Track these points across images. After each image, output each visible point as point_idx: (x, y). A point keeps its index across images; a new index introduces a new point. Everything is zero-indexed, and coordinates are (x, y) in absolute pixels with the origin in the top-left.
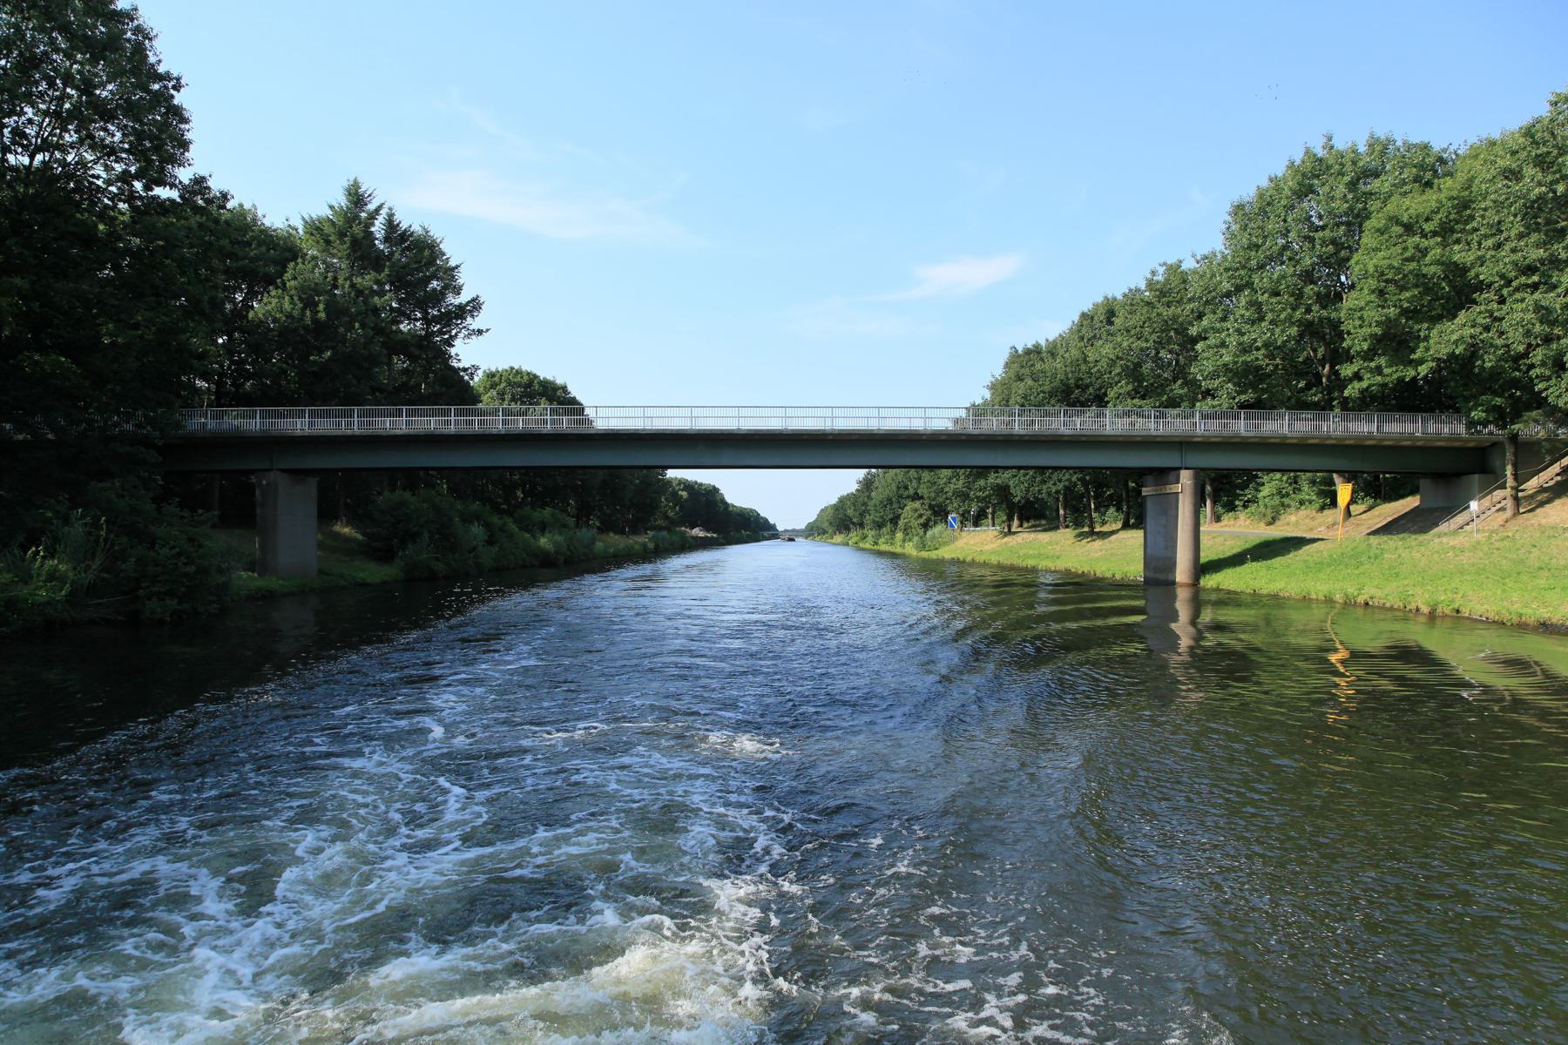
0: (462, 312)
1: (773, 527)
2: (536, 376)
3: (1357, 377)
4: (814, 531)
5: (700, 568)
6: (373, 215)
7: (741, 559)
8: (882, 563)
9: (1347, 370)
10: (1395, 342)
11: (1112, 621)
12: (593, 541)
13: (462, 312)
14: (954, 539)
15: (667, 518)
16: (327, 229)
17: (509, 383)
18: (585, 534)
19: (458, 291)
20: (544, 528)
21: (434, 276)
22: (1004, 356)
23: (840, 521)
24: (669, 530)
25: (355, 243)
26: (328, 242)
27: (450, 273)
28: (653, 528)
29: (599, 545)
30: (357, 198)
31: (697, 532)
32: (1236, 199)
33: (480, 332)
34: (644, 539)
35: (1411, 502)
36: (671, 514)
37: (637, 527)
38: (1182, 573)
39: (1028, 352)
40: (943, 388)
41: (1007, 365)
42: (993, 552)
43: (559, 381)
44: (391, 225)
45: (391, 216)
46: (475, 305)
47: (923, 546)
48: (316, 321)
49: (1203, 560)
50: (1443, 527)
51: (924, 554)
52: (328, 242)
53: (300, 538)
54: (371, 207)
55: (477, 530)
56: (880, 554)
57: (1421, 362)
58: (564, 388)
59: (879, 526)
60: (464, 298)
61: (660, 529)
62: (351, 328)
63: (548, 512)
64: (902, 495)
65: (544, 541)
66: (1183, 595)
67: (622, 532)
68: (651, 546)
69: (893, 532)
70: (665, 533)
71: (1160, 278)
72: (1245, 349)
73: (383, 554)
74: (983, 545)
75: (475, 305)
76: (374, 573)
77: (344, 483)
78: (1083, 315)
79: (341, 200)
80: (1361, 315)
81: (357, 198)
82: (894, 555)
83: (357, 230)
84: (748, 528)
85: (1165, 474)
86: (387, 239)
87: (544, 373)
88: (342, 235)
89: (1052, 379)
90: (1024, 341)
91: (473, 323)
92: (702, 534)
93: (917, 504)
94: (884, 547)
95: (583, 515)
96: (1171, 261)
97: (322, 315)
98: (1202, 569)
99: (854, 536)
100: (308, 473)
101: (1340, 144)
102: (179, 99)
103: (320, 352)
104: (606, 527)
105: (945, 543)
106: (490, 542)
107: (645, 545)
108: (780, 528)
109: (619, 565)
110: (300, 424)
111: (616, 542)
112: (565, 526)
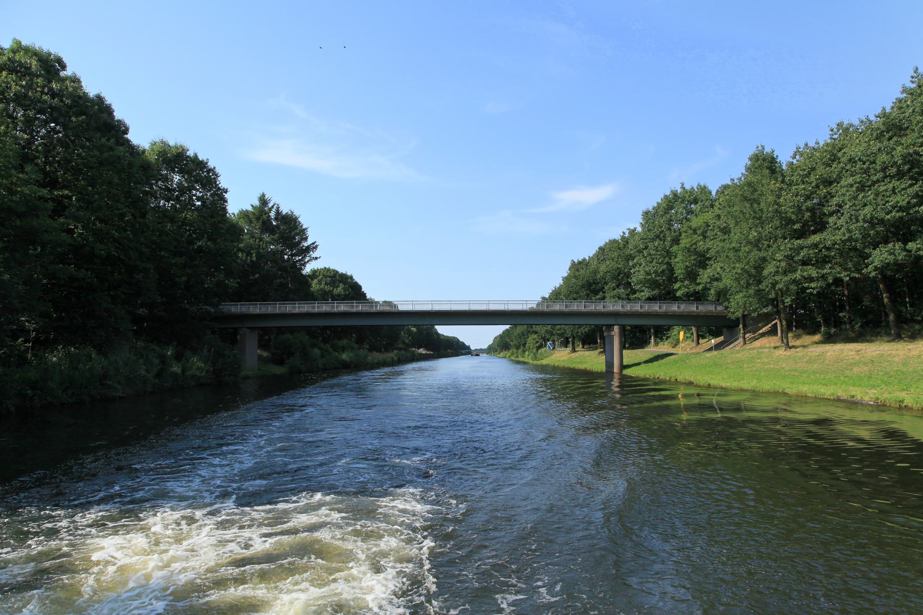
0: (308, 249)
1: (468, 348)
2: (337, 272)
3: (680, 288)
4: (491, 350)
5: (420, 369)
6: (270, 209)
7: (447, 369)
8: (519, 366)
9: (676, 286)
10: (692, 276)
11: (656, 404)
12: (366, 356)
13: (308, 249)
14: (552, 354)
15: (404, 343)
16: (251, 216)
17: (324, 276)
18: (362, 352)
19: (306, 239)
20: (343, 349)
21: (298, 234)
22: (569, 264)
23: (501, 346)
24: (405, 350)
25: (264, 223)
26: (251, 222)
27: (303, 231)
28: (396, 349)
29: (369, 358)
30: (263, 201)
31: (422, 351)
32: (645, 209)
33: (316, 258)
34: (392, 355)
35: (721, 338)
36: (407, 341)
37: (387, 348)
38: (616, 369)
39: (580, 263)
40: (532, 284)
41: (570, 269)
42: (564, 361)
43: (349, 274)
44: (278, 213)
45: (278, 208)
46: (313, 247)
47: (535, 358)
48: (252, 261)
49: (625, 363)
50: (727, 348)
51: (535, 362)
52: (251, 222)
53: (252, 355)
54: (270, 205)
55: (316, 351)
56: (518, 362)
57: (699, 284)
58: (351, 277)
59: (518, 348)
60: (309, 242)
61: (401, 349)
62: (266, 264)
63: (345, 342)
64: (524, 335)
65: (344, 356)
66: (616, 376)
67: (380, 351)
68: (396, 358)
69: (524, 351)
70: (403, 352)
71: (627, 235)
72: (648, 274)
73: (281, 363)
74: (561, 357)
75: (313, 247)
76: (278, 370)
77: (271, 334)
78: (600, 248)
79: (257, 203)
80: (680, 265)
81: (263, 201)
82: (524, 363)
83: (265, 217)
84: (456, 348)
85: (610, 327)
86: (276, 219)
87: (341, 270)
88: (258, 219)
89: (586, 281)
90: (578, 258)
91: (314, 255)
92: (424, 352)
93: (535, 336)
94: (521, 359)
95: (360, 341)
96: (632, 228)
97: (254, 259)
98: (623, 367)
99: (508, 353)
100: (256, 328)
101: (688, 187)
102: (226, 196)
103: (254, 275)
104: (372, 349)
105: (547, 357)
106: (322, 356)
107: (392, 358)
108: (472, 348)
109: (378, 368)
110: (256, 309)
111: (376, 356)
112: (353, 348)
